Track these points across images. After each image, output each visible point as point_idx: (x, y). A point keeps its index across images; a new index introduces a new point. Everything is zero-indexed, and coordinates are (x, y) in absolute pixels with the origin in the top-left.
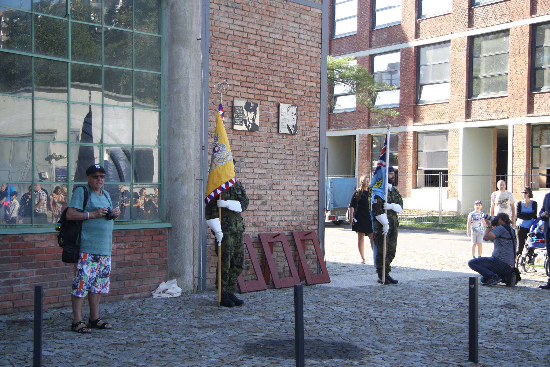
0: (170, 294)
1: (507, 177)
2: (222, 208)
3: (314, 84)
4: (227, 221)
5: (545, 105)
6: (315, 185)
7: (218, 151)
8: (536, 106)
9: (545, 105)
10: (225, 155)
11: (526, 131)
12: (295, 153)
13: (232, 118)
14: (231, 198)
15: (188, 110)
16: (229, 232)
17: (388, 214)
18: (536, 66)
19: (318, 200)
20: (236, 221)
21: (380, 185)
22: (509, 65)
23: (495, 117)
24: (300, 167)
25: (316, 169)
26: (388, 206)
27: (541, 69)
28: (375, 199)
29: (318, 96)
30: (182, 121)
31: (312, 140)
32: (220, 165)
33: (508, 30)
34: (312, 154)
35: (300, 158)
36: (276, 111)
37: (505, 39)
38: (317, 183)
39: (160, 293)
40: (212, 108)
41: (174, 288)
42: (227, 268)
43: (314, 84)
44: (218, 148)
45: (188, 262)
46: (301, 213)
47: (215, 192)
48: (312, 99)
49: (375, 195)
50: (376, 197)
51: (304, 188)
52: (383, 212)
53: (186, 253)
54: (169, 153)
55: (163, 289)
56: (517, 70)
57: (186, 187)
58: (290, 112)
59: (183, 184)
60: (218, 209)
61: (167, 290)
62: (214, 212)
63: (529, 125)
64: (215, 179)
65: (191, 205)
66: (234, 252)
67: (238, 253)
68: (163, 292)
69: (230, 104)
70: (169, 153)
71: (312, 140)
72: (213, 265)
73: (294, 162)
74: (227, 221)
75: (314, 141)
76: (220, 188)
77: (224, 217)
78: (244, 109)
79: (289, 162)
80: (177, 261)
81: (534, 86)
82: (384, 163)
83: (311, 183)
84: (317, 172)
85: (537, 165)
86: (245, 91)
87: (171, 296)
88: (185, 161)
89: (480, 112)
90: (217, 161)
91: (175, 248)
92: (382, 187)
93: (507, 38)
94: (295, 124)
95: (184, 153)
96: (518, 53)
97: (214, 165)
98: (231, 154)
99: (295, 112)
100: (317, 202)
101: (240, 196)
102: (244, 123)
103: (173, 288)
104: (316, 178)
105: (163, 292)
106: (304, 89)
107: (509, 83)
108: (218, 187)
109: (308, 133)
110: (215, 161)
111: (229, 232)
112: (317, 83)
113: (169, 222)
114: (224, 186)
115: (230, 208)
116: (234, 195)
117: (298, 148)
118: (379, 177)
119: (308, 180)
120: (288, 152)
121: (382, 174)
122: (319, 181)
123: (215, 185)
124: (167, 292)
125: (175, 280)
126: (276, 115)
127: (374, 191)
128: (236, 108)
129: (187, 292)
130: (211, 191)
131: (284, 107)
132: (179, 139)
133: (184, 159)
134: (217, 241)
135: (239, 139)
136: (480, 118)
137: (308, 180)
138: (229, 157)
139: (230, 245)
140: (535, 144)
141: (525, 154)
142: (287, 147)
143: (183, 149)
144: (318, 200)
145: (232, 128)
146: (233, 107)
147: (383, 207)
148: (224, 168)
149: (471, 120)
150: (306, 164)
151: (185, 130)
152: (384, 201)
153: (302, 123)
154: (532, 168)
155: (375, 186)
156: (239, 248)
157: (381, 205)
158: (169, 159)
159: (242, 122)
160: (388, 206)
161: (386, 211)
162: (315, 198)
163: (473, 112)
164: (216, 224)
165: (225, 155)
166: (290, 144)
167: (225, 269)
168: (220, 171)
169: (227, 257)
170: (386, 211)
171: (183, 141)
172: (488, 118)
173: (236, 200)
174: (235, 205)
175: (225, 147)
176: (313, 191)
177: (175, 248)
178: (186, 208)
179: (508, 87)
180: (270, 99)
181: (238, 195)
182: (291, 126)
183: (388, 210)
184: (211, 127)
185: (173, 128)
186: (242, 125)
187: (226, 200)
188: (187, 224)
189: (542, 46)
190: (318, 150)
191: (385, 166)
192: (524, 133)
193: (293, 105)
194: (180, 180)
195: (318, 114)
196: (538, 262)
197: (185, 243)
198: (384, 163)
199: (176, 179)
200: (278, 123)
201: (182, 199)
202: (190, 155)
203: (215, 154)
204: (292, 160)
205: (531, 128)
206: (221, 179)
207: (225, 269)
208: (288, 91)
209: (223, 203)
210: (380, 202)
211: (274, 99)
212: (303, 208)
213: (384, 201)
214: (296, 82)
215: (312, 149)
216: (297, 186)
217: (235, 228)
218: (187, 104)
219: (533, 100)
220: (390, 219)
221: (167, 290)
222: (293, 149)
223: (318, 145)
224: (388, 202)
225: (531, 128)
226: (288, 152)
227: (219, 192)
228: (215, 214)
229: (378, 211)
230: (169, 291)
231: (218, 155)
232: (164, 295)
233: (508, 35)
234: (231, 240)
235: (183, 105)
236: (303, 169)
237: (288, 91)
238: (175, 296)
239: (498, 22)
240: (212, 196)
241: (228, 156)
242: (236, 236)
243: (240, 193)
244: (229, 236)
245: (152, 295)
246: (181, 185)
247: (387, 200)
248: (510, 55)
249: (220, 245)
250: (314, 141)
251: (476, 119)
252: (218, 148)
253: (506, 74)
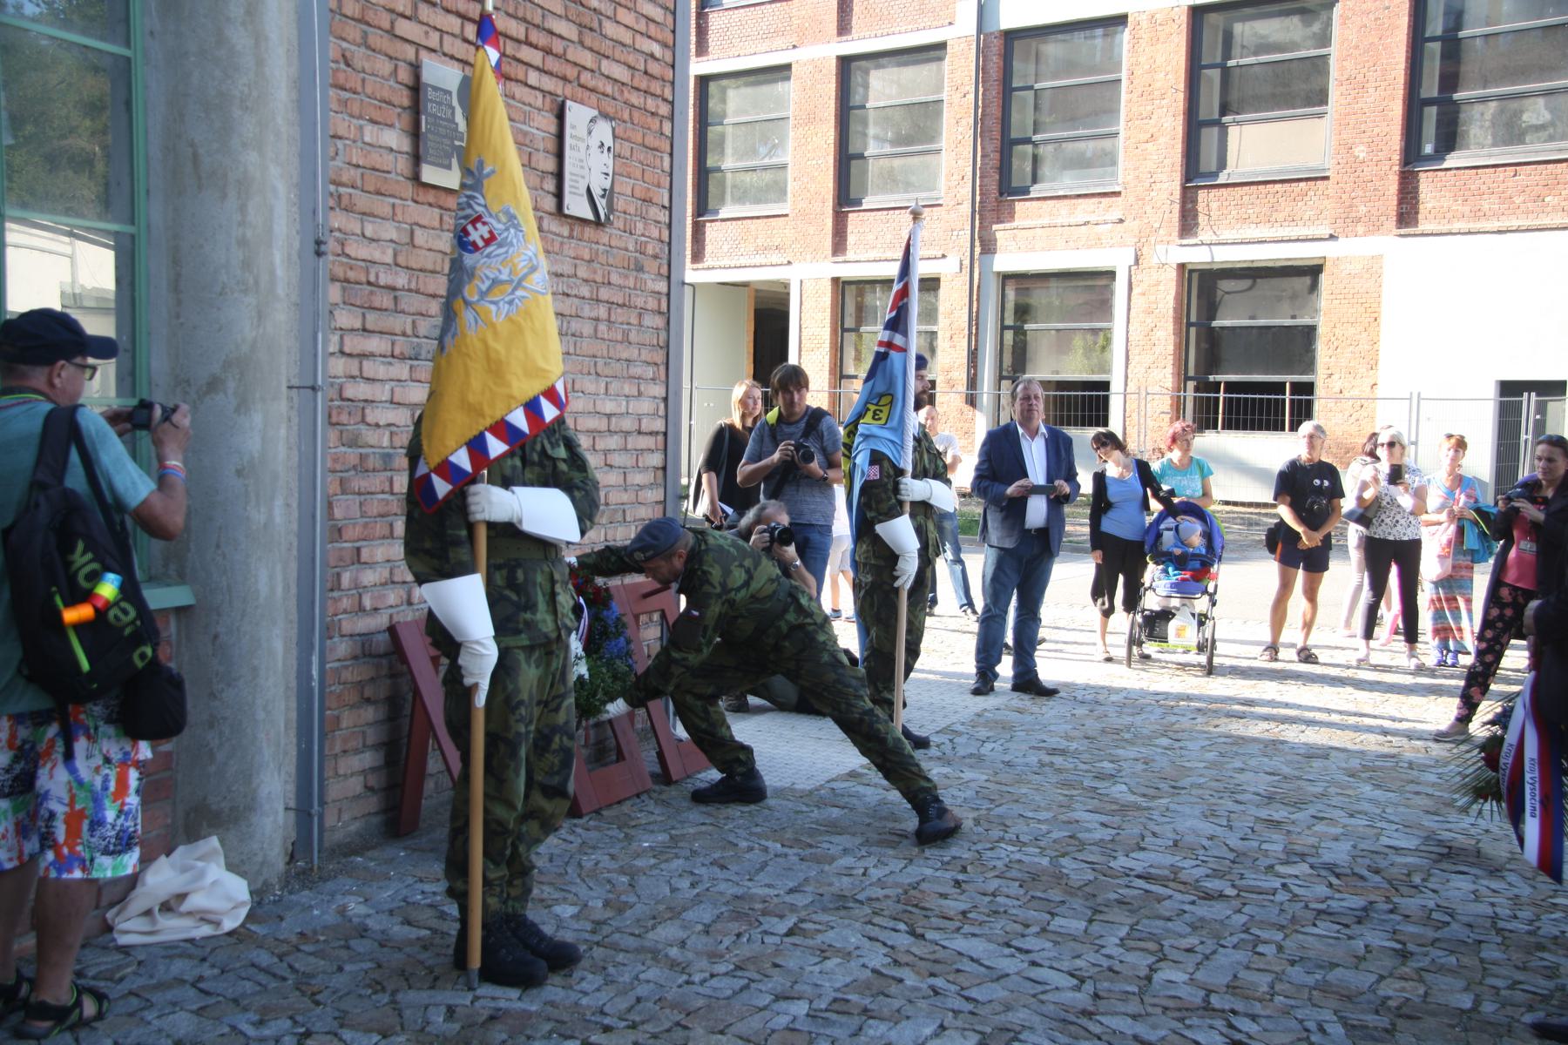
0: (204, 917)
1: (1106, 399)
2: (491, 525)
3: (656, 49)
4: (512, 583)
5: (871, 237)
6: (656, 414)
7: (488, 242)
8: (851, 239)
9: (871, 237)
10: (522, 265)
11: (829, 295)
12: (604, 293)
13: (415, 134)
14: (528, 475)
15: (260, 63)
16: (524, 640)
17: (912, 516)
18: (852, 150)
19: (664, 469)
20: (553, 582)
21: (884, 416)
22: (790, 145)
23: (758, 260)
24: (619, 347)
25: (659, 357)
26: (915, 489)
27: (861, 157)
28: (872, 463)
29: (668, 94)
30: (237, 113)
31: (650, 250)
32: (496, 312)
33: (788, 67)
34: (652, 304)
35: (619, 315)
36: (553, 129)
37: (780, 87)
38: (662, 406)
39: (148, 913)
40: (341, 79)
41: (215, 883)
42: (511, 805)
43: (656, 49)
44: (483, 230)
45: (267, 753)
46: (619, 517)
47: (477, 447)
48: (651, 104)
49: (873, 452)
50: (876, 458)
51: (628, 424)
52: (894, 512)
53: (261, 715)
54: (176, 261)
55: (163, 895)
56: (809, 156)
57: (258, 418)
58: (594, 143)
59: (243, 406)
60: (471, 527)
61: (182, 897)
62: (457, 543)
63: (835, 280)
64: (476, 384)
65: (279, 503)
66: (538, 730)
67: (555, 729)
68: (166, 907)
69: (405, 75)
70: (176, 261)
71: (650, 250)
72: (349, 746)
73: (602, 327)
74: (512, 583)
75: (656, 257)
76: (503, 429)
77: (499, 567)
78: (455, 103)
79: (587, 329)
80: (220, 756)
81: (846, 197)
82: (898, 340)
83: (645, 406)
84: (662, 368)
85: (850, 369)
86: (457, 31)
87: (206, 930)
88: (251, 300)
89: (725, 248)
90: (483, 295)
91: (213, 695)
92: (894, 423)
93: (786, 84)
94: (607, 185)
95: (247, 265)
96: (811, 119)
97: (467, 316)
98: (544, 264)
99: (609, 142)
100: (660, 473)
101: (563, 467)
102: (454, 162)
103: (210, 888)
104: (659, 390)
105: (166, 907)
106: (631, 59)
107: (791, 186)
108: (488, 422)
109: (640, 226)
110: (470, 293)
111: (524, 640)
112: (665, 45)
113: (182, 578)
114: (519, 419)
115: (528, 527)
116: (541, 464)
117: (615, 278)
118: (880, 388)
119: (640, 394)
120: (585, 291)
121: (891, 383)
122: (666, 400)
123: (475, 411)
124: (185, 907)
125: (214, 841)
126: (551, 145)
127: (866, 437)
128: (431, 94)
129: (267, 885)
130: (451, 443)
131: (577, 115)
132: (224, 196)
133: (245, 291)
134: (468, 681)
135: (436, 224)
136: (726, 262)
137: (640, 394)
138: (536, 276)
139: (525, 696)
140: (850, 323)
141: (827, 345)
142: (583, 272)
143: (243, 242)
144: (664, 469)
145: (416, 178)
146: (416, 88)
147: (896, 490)
148: (518, 330)
149: (705, 265)
150: (633, 336)
151: (252, 157)
152: (901, 472)
153: (624, 186)
154: (842, 377)
155: (868, 418)
156: (557, 709)
157: (890, 487)
158: (176, 286)
159: (450, 157)
160: (915, 489)
161: (907, 508)
162: (656, 460)
163: (709, 249)
164: (466, 602)
165: (522, 265)
166: (591, 261)
167: (500, 811)
168: (498, 346)
169: (514, 754)
170: (907, 508)
171: (243, 209)
172: (743, 261)
173: (546, 484)
174: (545, 512)
175: (517, 227)
176: (651, 433)
177: (213, 695)
178: (258, 516)
179: (789, 195)
180: (533, 78)
181: (554, 460)
182: (597, 192)
183: (913, 503)
184: (338, 163)
185: (192, 145)
186: (449, 167)
187: (506, 483)
188: (263, 588)
189: (863, 107)
190: (665, 290)
191: (903, 350)
192: (826, 299)
193: (605, 116)
194: (231, 385)
195: (667, 159)
196: (1178, 635)
197: (255, 670)
198: (898, 340)
199: (214, 385)
200: (559, 176)
201: (239, 473)
202: (272, 273)
203: (469, 259)
204: (597, 319)
205: (840, 286)
206: (509, 385)
207: (500, 811)
208: (587, 59)
209: (497, 503)
210: (889, 476)
211: (549, 84)
212: (625, 497)
213: (901, 472)
214: (610, 29)
215: (651, 285)
216: (609, 416)
217: (549, 618)
218: (259, 38)
219: (845, 226)
220: (920, 531)
221: (182, 897)
222: (599, 279)
223: (664, 270)
224: (914, 477)
225: (840, 286)
226: (585, 291)
227: (496, 447)
228: (463, 554)
229: (884, 507)
230: (196, 901)
231: (485, 265)
232: (174, 928)
233: (788, 78)
234: (529, 675)
235: (240, 38)
236: (625, 355)
237: (587, 59)
238: (229, 924)
239: (764, 47)
240: (457, 469)
241: (533, 269)
242: (549, 653)
243: (561, 452)
244: (521, 656)
245: (109, 929)
246: (237, 410)
247: (910, 469)
248: (791, 121)
249: (481, 700)
250: (656, 257)
251: (717, 264)
252: (483, 230)
253: (784, 167)
